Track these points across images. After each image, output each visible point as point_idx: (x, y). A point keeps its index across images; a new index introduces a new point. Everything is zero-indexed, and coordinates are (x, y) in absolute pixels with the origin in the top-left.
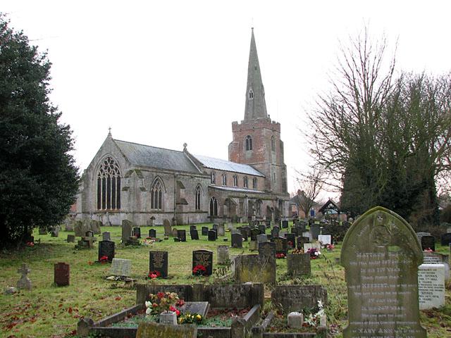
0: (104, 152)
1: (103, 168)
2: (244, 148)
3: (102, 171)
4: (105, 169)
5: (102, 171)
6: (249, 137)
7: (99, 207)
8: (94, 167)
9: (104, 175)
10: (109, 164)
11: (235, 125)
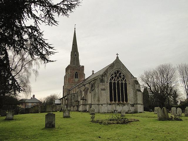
7: (111, 100)
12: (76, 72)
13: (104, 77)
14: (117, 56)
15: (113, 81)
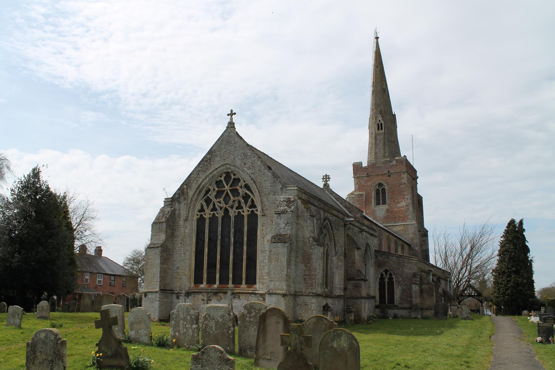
0: (216, 164)
1: (212, 195)
2: (373, 201)
3: (208, 201)
4: (218, 196)
5: (208, 201)
6: (380, 185)
7: (198, 280)
8: (191, 193)
9: (214, 209)
10: (227, 188)
11: (357, 167)
12: (380, 185)
13: (177, 204)
14: (231, 119)
15: (207, 214)
